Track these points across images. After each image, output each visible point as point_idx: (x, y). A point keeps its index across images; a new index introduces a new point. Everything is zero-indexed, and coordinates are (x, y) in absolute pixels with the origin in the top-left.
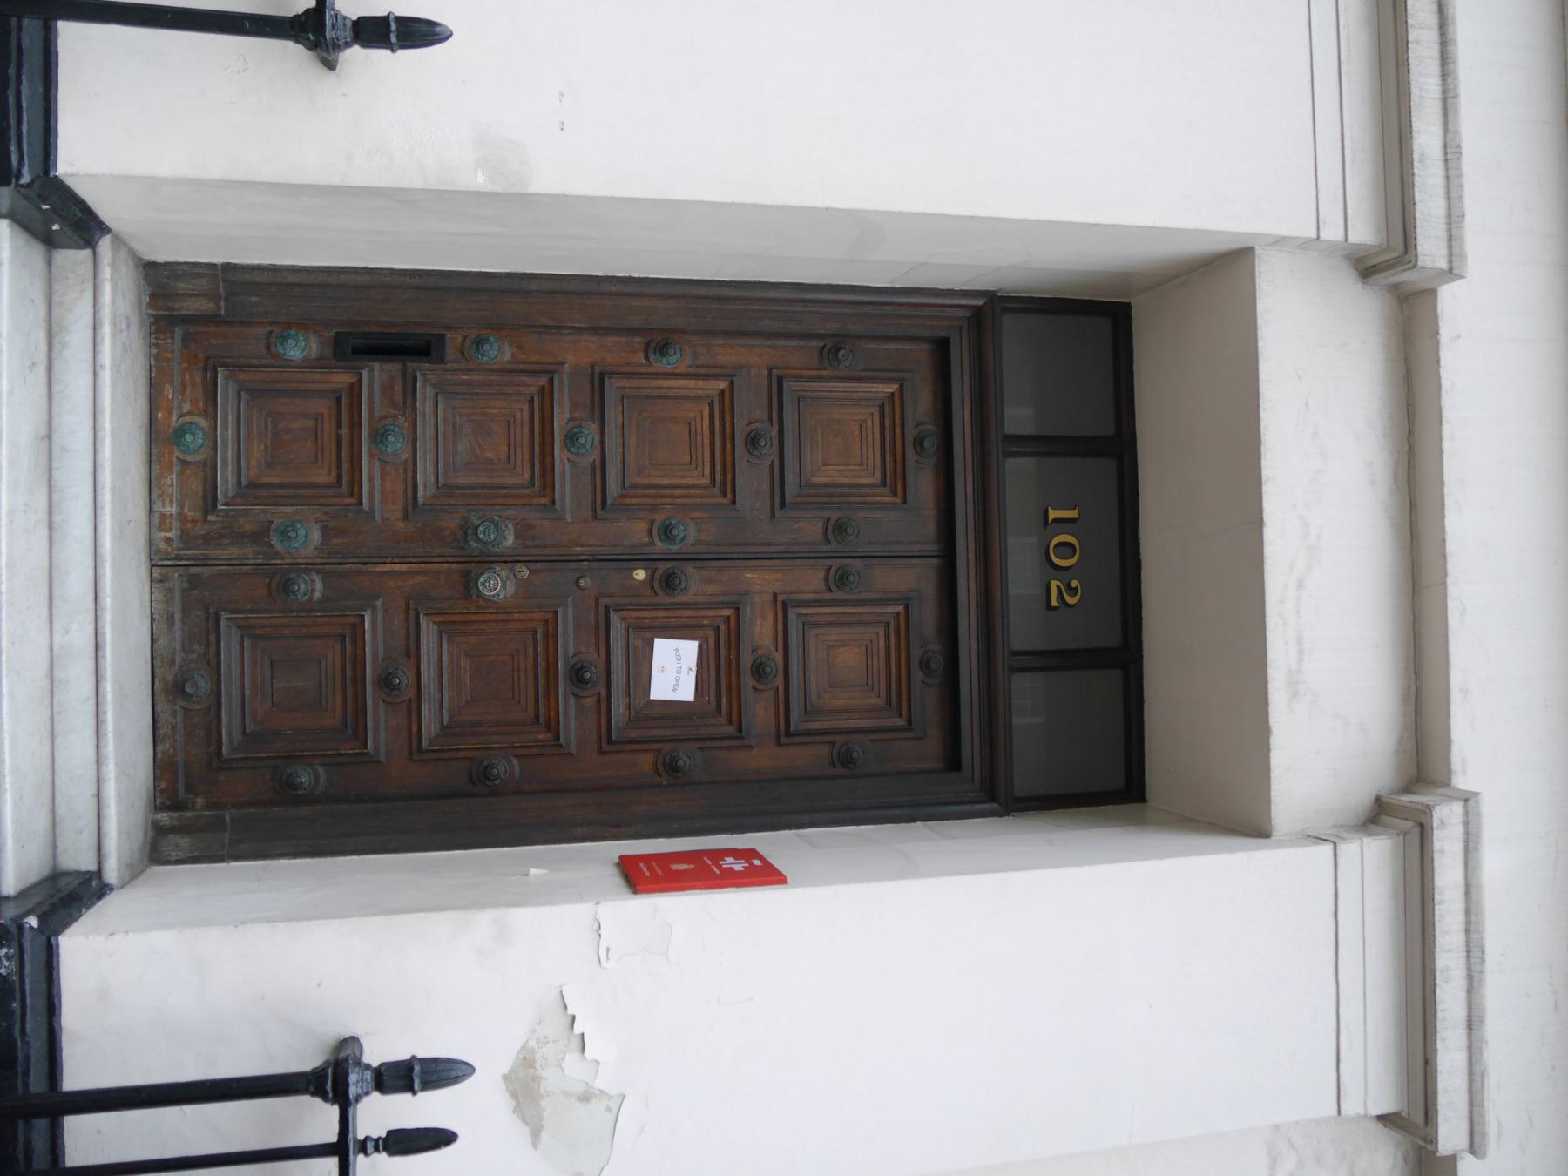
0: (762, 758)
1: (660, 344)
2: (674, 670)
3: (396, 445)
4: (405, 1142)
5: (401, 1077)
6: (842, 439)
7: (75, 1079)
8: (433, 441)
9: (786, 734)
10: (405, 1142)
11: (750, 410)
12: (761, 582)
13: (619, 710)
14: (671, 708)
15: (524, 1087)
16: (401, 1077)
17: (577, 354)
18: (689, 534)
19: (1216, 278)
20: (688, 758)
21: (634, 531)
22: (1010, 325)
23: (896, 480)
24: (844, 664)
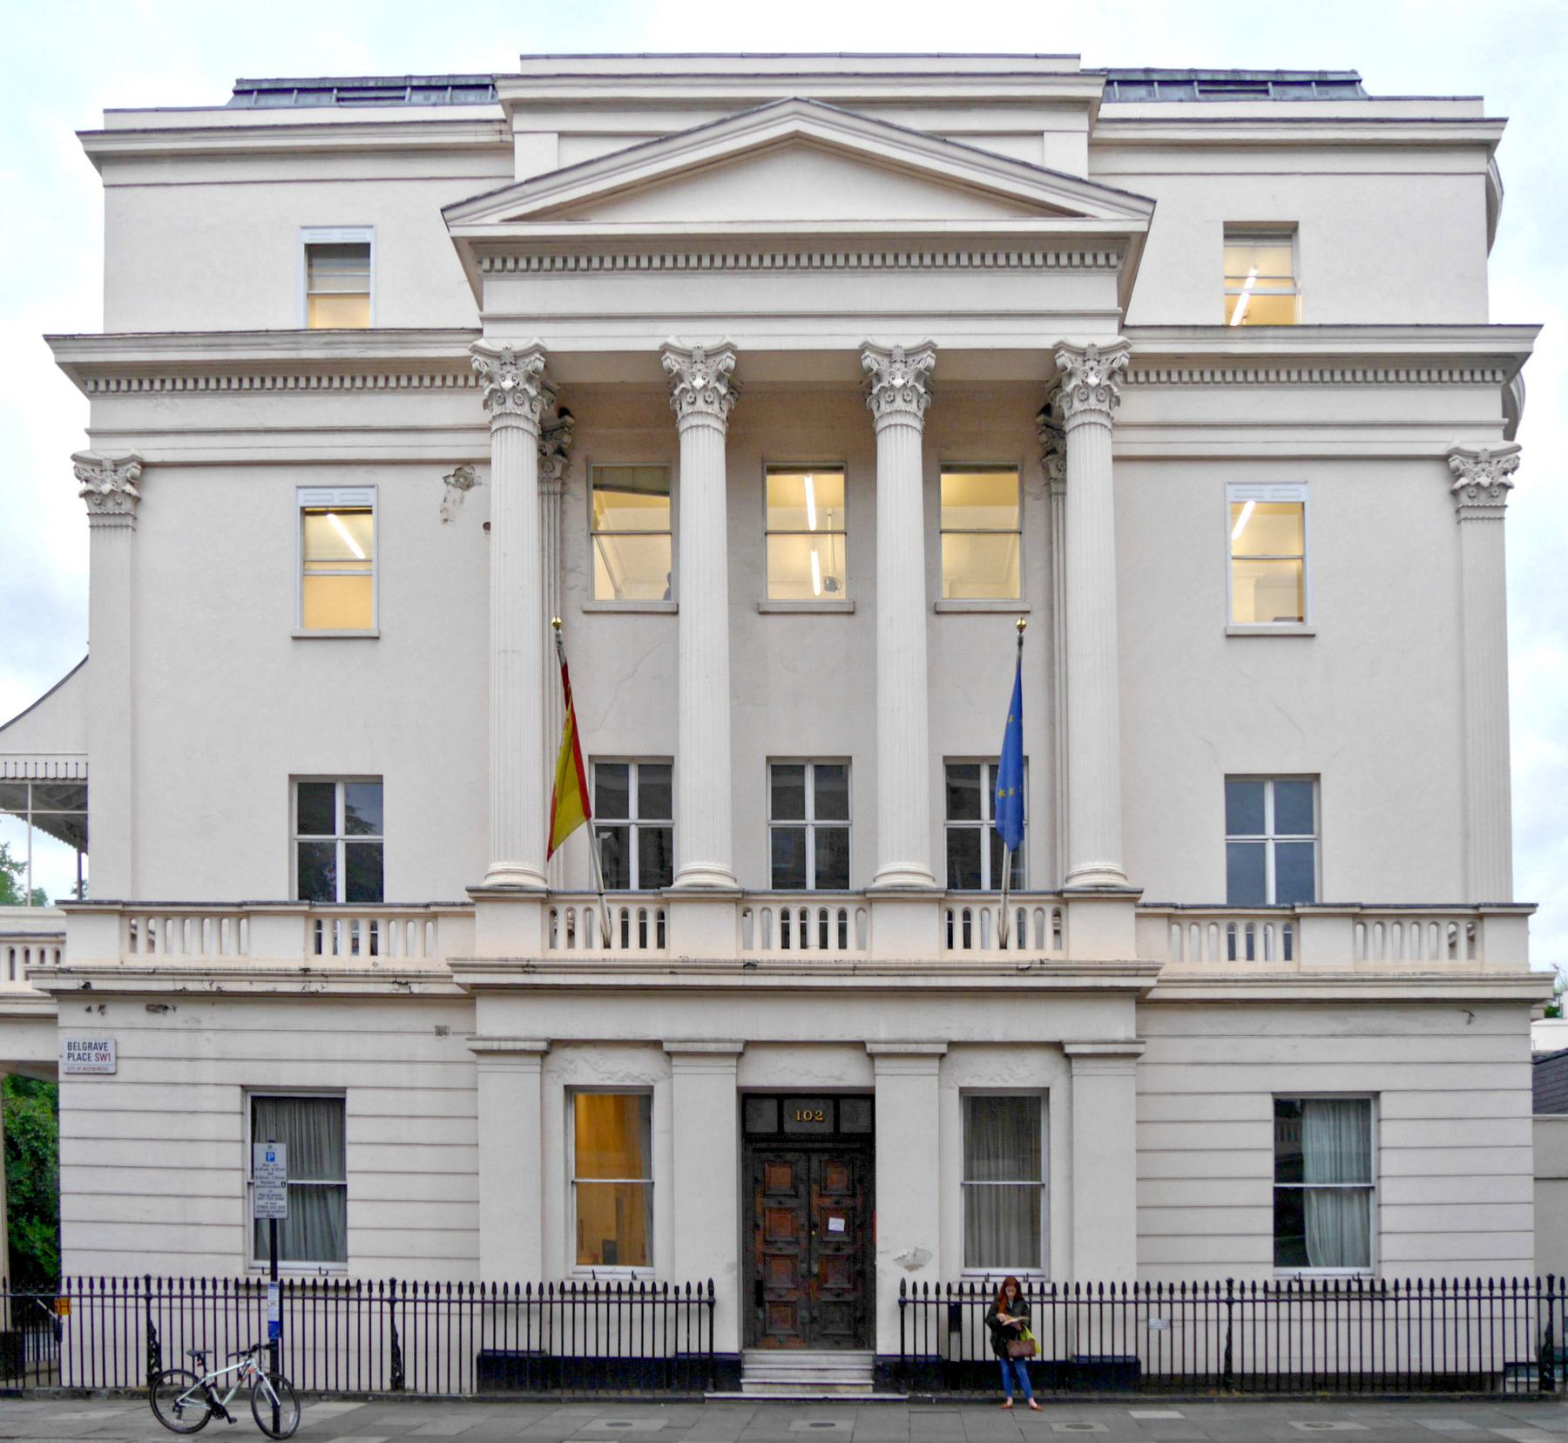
0: (859, 1201)
1: (757, 1226)
2: (836, 1224)
3: (783, 1292)
4: (1563, 1287)
5: (903, 1292)
6: (780, 1176)
7: (898, 1352)
8: (780, 1281)
9: (853, 1195)
10: (1563, 1287)
11: (772, 1203)
12: (815, 1201)
13: (846, 1239)
14: (846, 1226)
15: (912, 1268)
16: (903, 1292)
17: (760, 1246)
18: (803, 1220)
19: (748, 1099)
20: (858, 1222)
21: (803, 1235)
22: (752, 1128)
23: (789, 1164)
24: (838, 1179)
